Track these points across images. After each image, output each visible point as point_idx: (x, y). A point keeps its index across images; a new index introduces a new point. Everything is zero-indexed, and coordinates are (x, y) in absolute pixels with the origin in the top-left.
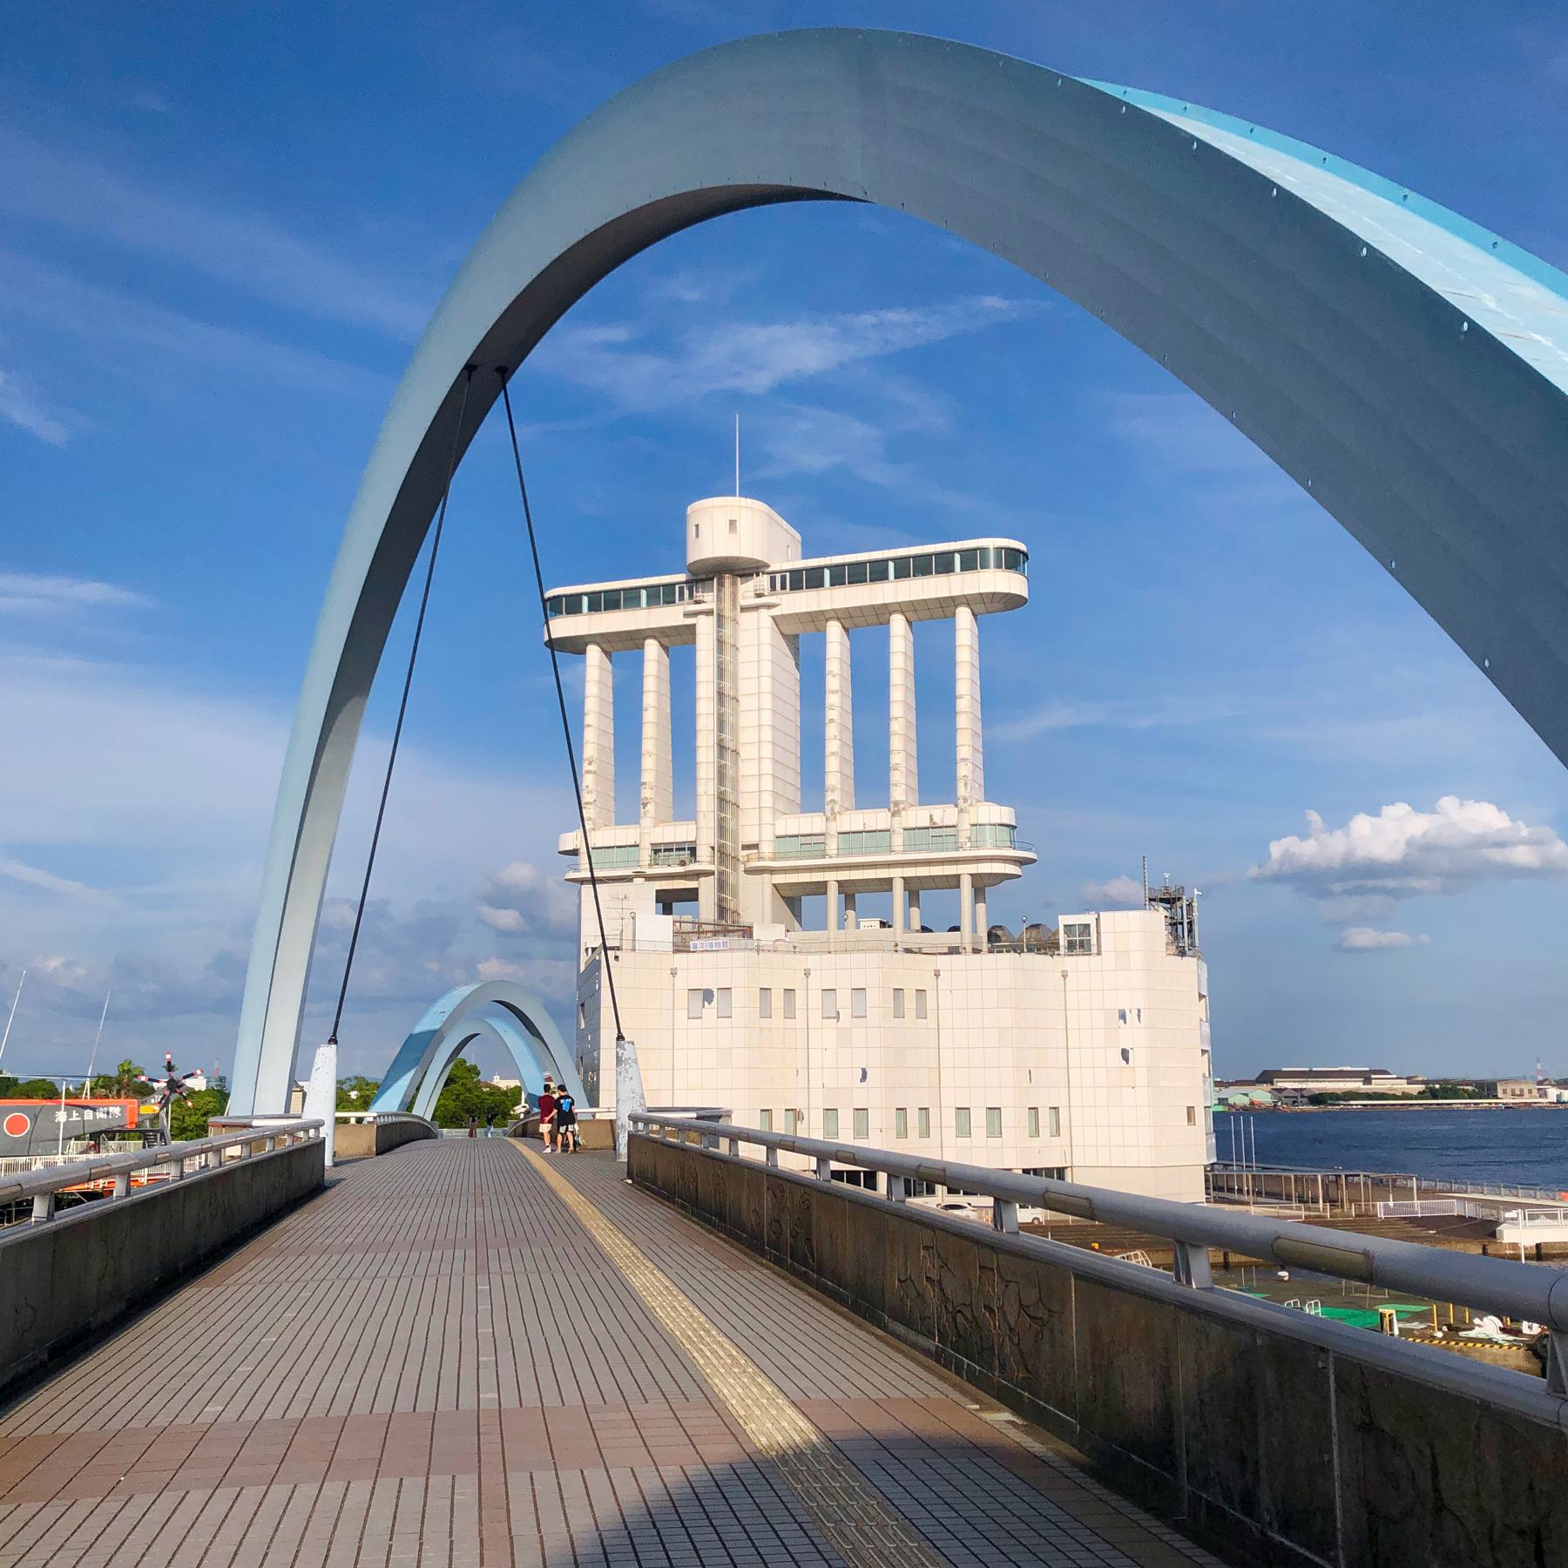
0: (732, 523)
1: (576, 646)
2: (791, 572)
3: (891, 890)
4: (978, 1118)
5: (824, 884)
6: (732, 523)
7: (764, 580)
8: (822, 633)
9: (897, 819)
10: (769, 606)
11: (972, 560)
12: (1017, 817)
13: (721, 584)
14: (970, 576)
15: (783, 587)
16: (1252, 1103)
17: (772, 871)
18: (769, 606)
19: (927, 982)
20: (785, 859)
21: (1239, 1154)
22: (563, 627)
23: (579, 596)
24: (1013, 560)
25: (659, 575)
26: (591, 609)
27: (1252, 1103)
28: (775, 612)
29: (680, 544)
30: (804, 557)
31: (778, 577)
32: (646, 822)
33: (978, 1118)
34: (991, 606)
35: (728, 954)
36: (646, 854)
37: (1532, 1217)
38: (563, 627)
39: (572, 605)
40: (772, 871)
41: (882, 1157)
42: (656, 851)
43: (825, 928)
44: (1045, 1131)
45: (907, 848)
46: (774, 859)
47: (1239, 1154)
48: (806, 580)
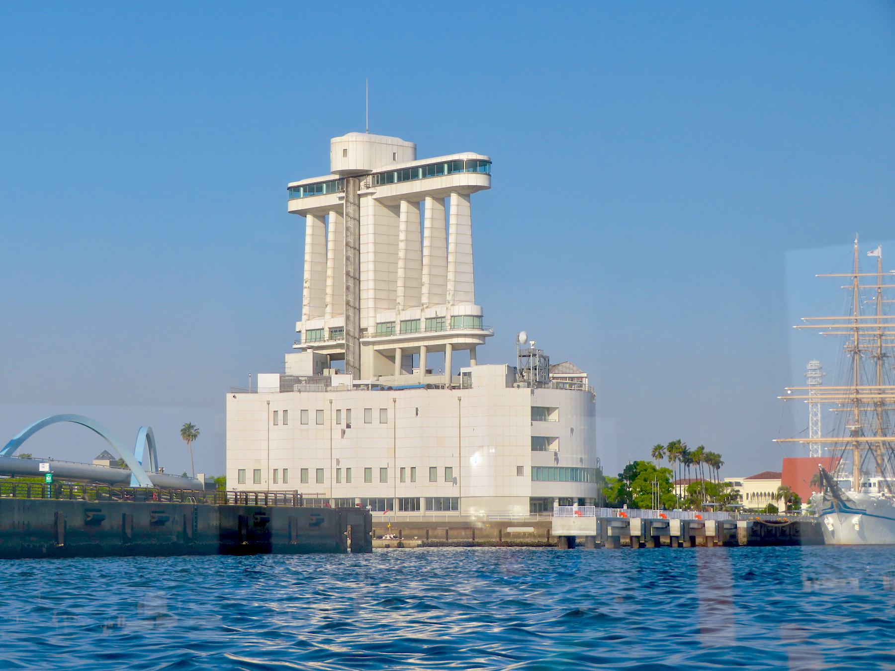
0: (345, 151)
1: (303, 213)
4: (376, 474)
6: (345, 151)
7: (370, 178)
10: (372, 194)
11: (455, 167)
13: (348, 182)
17: (374, 343)
18: (372, 194)
20: (381, 336)
22: (295, 205)
23: (442, 163)
24: (474, 166)
28: (375, 196)
29: (327, 161)
30: (415, 159)
32: (328, 316)
33: (376, 474)
34: (466, 192)
35: (307, 393)
36: (326, 334)
38: (295, 205)
40: (374, 343)
45: (331, 338)
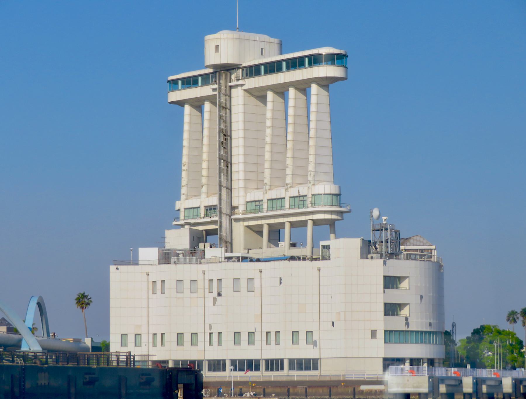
0: (217, 47)
1: (181, 103)
3: (307, 226)
5: (306, 222)
6: (217, 47)
7: (240, 71)
8: (182, 115)
9: (287, 193)
10: (242, 85)
11: (315, 60)
15: (247, 75)
17: (244, 220)
18: (242, 85)
19: (256, 275)
22: (175, 96)
24: (333, 59)
29: (201, 56)
30: (281, 53)
32: (203, 196)
34: (325, 83)
36: (202, 212)
38: (175, 96)
40: (244, 220)
41: (327, 379)
42: (207, 210)
43: (261, 248)
44: (158, 291)
45: (207, 215)
46: (245, 214)
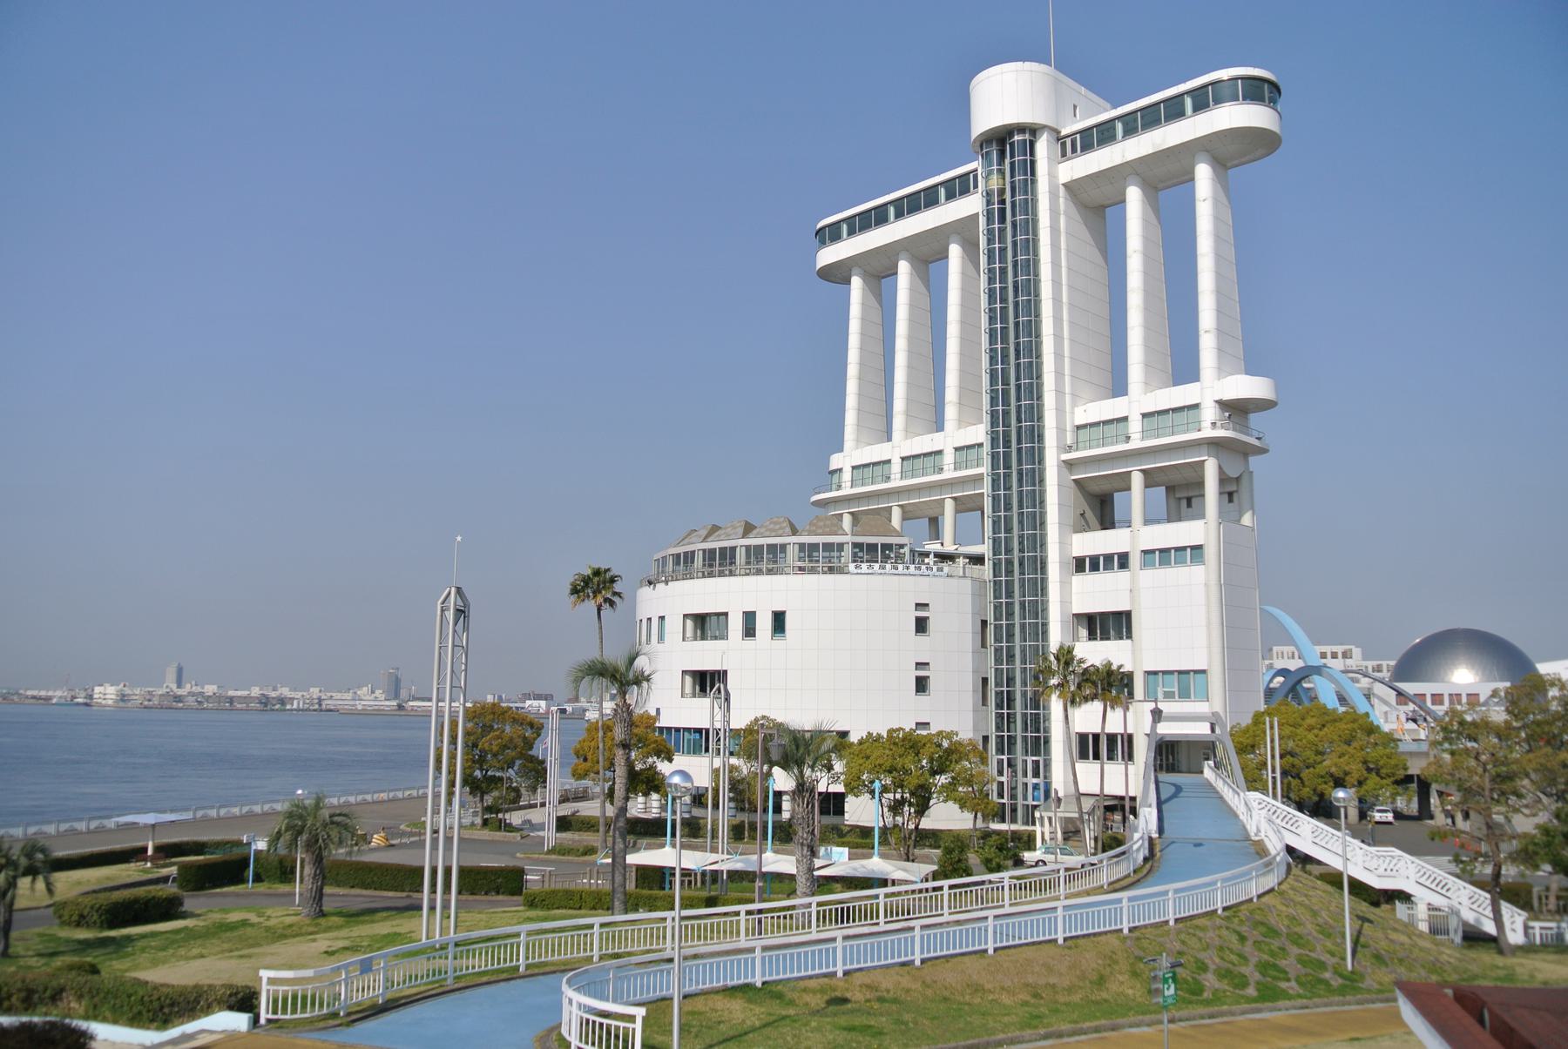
2: (1080, 132)
11: (1203, 99)
12: (1277, 388)
14: (1203, 117)
15: (1074, 150)
16: (1367, 714)
21: (448, 840)
22: (830, 255)
24: (1257, 90)
25: (1184, 81)
26: (1083, 150)
27: (1367, 714)
31: (1068, 141)
34: (1230, 152)
37: (844, 915)
38: (830, 255)
39: (832, 234)
45: (1145, 434)
47: (448, 840)
48: (1100, 135)
